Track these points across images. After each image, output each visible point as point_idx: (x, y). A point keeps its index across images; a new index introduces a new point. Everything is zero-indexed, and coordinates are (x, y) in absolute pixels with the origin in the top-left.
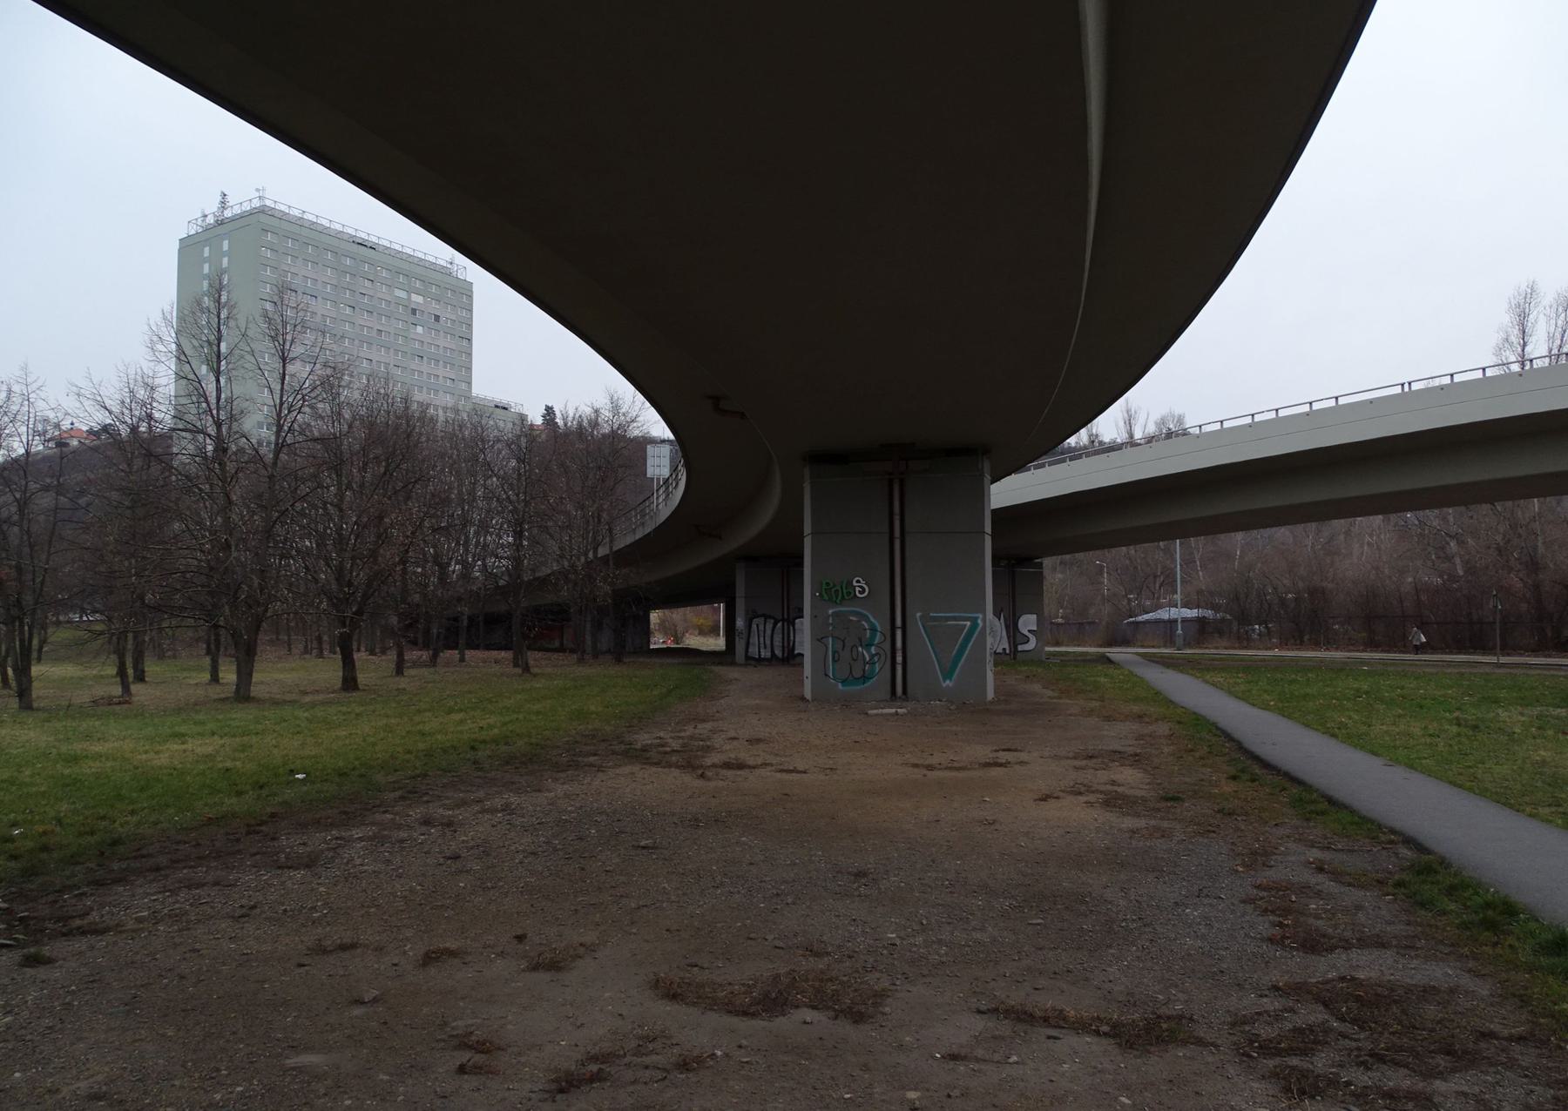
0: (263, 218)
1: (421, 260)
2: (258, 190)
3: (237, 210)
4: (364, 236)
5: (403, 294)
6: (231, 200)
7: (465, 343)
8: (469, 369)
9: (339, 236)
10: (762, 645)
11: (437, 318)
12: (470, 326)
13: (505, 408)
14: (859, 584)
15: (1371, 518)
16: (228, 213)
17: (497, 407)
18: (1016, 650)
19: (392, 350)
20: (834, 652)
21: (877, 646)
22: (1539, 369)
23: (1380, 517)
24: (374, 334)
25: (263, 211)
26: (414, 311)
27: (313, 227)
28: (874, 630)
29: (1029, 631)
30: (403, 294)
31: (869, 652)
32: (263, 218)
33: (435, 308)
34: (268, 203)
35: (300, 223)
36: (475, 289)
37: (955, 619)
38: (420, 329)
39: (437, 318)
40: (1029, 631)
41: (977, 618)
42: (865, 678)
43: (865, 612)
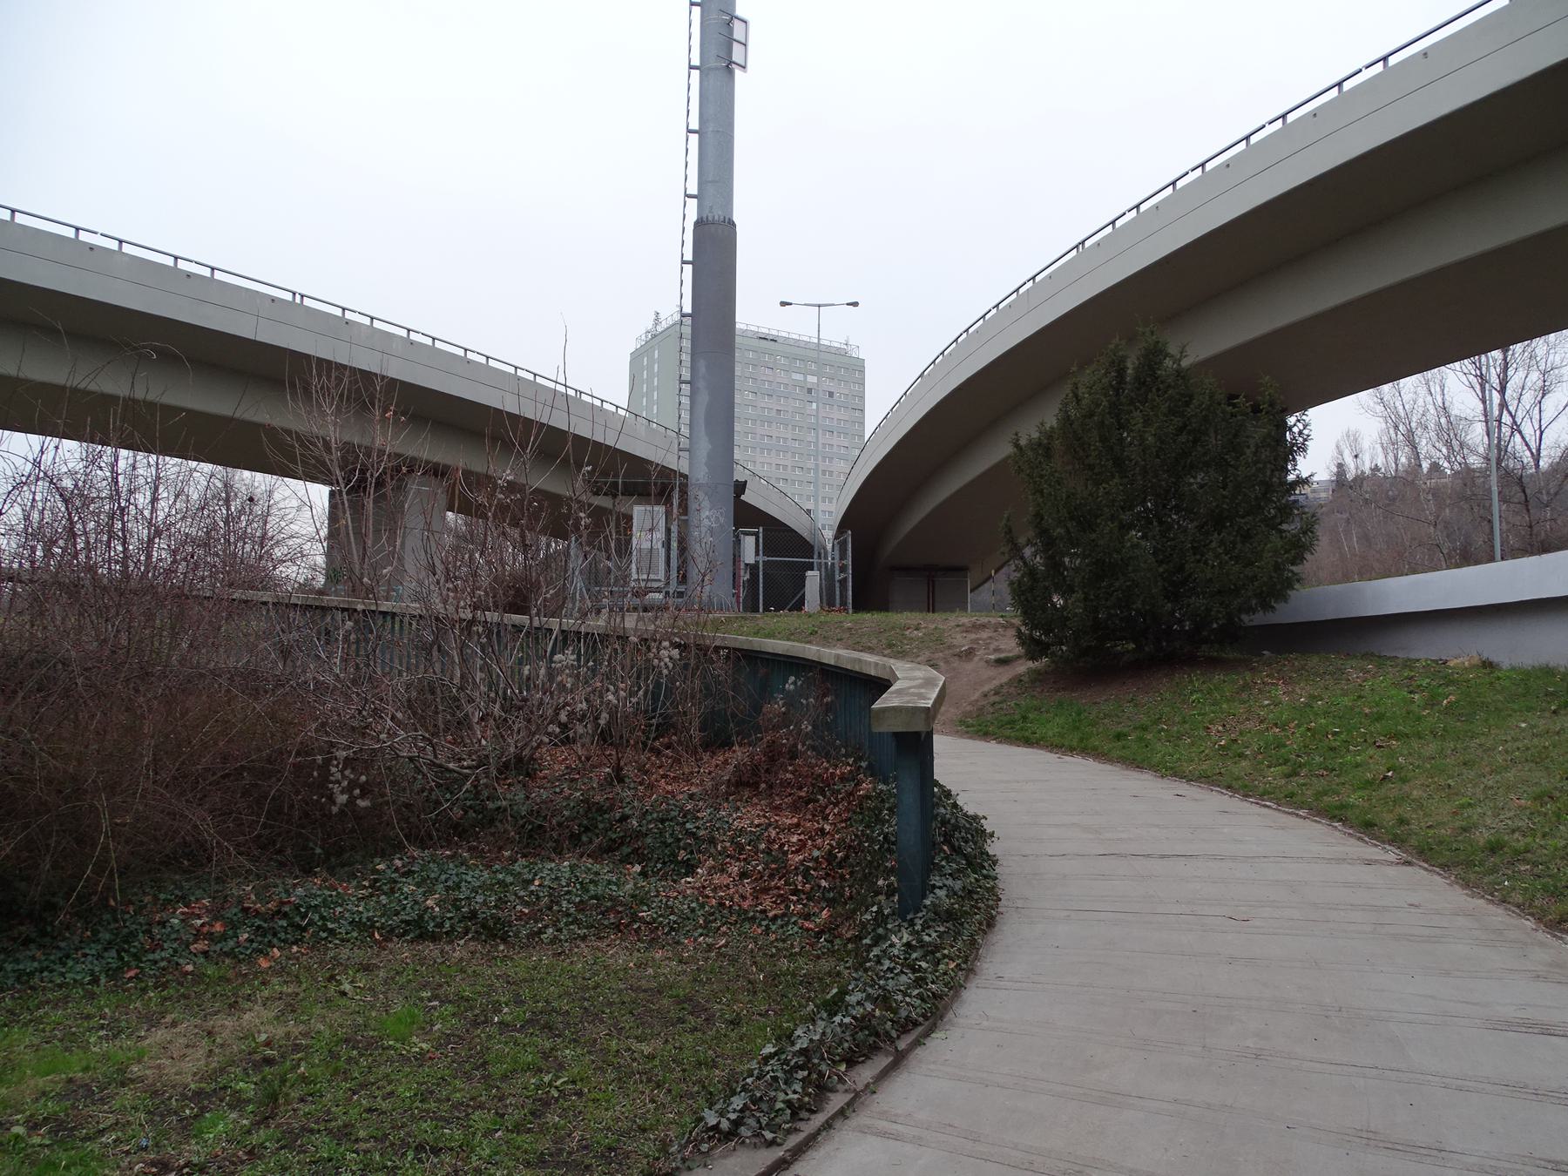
3: (664, 325)
5: (799, 377)
6: (662, 317)
11: (831, 394)
12: (862, 398)
16: (660, 329)
24: (774, 413)
26: (810, 391)
30: (799, 377)
33: (829, 385)
39: (831, 394)
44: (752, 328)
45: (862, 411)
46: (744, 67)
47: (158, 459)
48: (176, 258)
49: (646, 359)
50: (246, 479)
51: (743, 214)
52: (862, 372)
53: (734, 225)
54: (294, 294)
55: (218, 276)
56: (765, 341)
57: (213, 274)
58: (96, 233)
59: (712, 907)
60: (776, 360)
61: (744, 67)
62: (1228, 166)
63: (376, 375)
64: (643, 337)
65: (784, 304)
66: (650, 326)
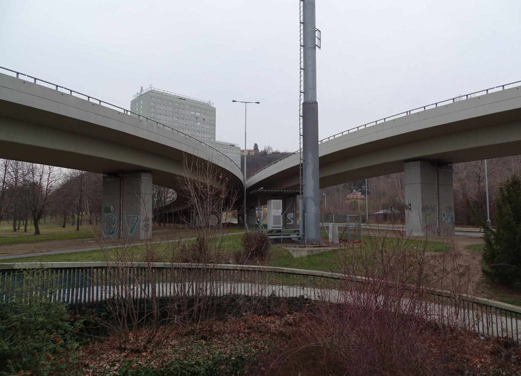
0: (151, 94)
1: (199, 102)
2: (150, 85)
3: (145, 92)
4: (181, 96)
5: (193, 113)
6: (144, 89)
7: (213, 127)
8: (215, 135)
9: (174, 97)
10: (200, 223)
11: (204, 119)
12: (215, 121)
13: (233, 146)
14: (112, 208)
15: (372, 178)
16: (143, 93)
17: (230, 145)
18: (286, 225)
19: (190, 130)
20: (106, 226)
21: (116, 224)
22: (345, 135)
23: (383, 176)
24: (184, 125)
25: (152, 91)
26: (197, 118)
27: (167, 95)
28: (115, 220)
29: (291, 218)
30: (193, 113)
31: (114, 226)
32: (151, 94)
33: (204, 116)
34: (153, 89)
35: (162, 94)
36: (216, 110)
37: (133, 217)
38: (199, 123)
39: (204, 119)
40: (291, 218)
41: (138, 217)
42: (113, 233)
43: (112, 215)
44: (177, 95)
45: (215, 126)
46: (320, 48)
47: (6, 161)
48: (35, 79)
49: (137, 103)
50: (34, 165)
51: (320, 99)
52: (215, 112)
53: (317, 103)
54: (125, 110)
55: (102, 104)
56: (181, 100)
57: (71, 93)
58: (25, 75)
59: (237, 368)
60: (185, 106)
61: (320, 48)
62: (479, 98)
63: (207, 161)
64: (136, 95)
65: (234, 101)
66: (139, 92)
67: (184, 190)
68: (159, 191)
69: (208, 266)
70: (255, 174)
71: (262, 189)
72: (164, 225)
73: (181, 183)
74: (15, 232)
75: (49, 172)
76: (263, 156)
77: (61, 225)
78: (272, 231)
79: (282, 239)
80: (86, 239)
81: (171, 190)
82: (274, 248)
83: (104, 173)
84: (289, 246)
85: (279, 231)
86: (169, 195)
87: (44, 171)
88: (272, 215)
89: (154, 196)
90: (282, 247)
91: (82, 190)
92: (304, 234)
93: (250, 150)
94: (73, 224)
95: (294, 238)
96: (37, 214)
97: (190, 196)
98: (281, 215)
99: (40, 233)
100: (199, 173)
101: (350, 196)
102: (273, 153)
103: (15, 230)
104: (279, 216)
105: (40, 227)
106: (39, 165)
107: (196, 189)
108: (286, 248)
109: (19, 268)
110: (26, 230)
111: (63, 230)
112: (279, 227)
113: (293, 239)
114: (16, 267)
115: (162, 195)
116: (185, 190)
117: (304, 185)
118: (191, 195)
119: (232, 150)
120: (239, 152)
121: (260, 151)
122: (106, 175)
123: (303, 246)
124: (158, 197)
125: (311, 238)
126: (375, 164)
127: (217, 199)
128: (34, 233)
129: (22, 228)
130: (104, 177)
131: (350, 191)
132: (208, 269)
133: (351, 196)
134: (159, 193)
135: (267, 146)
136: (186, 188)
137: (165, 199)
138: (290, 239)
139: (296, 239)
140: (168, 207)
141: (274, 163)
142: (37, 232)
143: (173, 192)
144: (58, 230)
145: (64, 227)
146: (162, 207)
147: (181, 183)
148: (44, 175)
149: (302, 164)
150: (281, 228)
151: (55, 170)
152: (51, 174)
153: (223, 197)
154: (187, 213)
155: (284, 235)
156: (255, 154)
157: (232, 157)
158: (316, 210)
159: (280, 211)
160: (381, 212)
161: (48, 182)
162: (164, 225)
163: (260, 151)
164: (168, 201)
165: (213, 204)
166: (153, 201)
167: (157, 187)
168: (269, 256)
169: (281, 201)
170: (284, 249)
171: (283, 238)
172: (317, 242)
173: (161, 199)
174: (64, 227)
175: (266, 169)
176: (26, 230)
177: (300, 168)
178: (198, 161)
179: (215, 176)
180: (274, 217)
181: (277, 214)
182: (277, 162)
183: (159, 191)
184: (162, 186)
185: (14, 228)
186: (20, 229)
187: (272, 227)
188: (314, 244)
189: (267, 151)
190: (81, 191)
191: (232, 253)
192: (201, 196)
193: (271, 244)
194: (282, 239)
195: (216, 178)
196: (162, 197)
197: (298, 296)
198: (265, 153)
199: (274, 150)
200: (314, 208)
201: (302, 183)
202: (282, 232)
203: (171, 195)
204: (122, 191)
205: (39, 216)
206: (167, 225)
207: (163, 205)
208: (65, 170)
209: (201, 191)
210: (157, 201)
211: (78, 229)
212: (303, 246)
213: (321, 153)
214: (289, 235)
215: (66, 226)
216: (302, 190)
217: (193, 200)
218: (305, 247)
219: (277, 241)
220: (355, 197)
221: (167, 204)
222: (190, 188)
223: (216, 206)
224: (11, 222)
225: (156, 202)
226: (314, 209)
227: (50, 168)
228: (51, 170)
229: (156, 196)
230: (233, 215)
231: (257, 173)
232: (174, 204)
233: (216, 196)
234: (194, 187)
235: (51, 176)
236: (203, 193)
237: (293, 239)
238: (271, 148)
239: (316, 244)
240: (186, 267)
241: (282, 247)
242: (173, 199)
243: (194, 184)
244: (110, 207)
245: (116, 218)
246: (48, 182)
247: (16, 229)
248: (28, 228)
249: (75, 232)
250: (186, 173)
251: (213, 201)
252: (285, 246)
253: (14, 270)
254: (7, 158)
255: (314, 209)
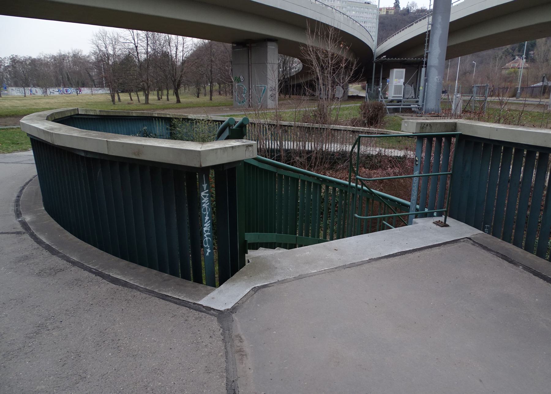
13: (368, 3)
14: (241, 77)
17: (365, 3)
50: (170, 35)
67: (307, 59)
68: (285, 60)
69: (325, 126)
70: (387, 40)
71: (384, 58)
72: (290, 97)
73: (304, 52)
74: (159, 101)
75: (183, 43)
76: (404, 15)
77: (195, 95)
78: (392, 101)
79: (400, 108)
80: (221, 107)
81: (296, 59)
82: (389, 117)
83: (233, 43)
84: (406, 115)
85: (399, 101)
86: (294, 65)
87: (179, 42)
88: (394, 85)
89: (279, 67)
90: (399, 116)
91: (212, 60)
92: (423, 104)
93: (389, 8)
94: (205, 95)
95: (415, 108)
96: (176, 84)
97: (312, 65)
98: (403, 84)
99: (181, 102)
100: (321, 42)
101: (511, 65)
102: (418, 11)
103: (159, 99)
104: (401, 86)
105: (180, 97)
106: (173, 36)
107: (318, 58)
108: (403, 117)
109: (191, 118)
110: (168, 100)
111: (198, 100)
112: (400, 97)
113: (413, 109)
114: (189, 117)
115: (287, 65)
116: (308, 60)
117: (429, 52)
118: (313, 64)
119: (366, 10)
120: (375, 11)
121: (401, 9)
122: (235, 45)
123: (420, 115)
124: (283, 67)
125: (430, 108)
126: (527, 25)
127: (337, 68)
128: (176, 102)
129: (164, 97)
130: (233, 47)
131: (512, 58)
132: (323, 129)
133: (512, 64)
134: (284, 63)
135: (410, 2)
136: (308, 58)
137: (290, 69)
138: (410, 109)
139: (416, 109)
140: (292, 78)
141: (409, 27)
142: (178, 101)
143: (299, 62)
144: (194, 100)
145: (198, 97)
146: (288, 78)
147: (304, 52)
148: (179, 46)
149: (429, 31)
150: (402, 98)
151: (188, 40)
152: (185, 44)
153: (344, 65)
154: (312, 85)
155: (403, 105)
156: (395, 13)
157: (367, 18)
158: (438, 80)
159: (403, 80)
160: (540, 84)
161: (183, 53)
162: (290, 97)
163: (401, 9)
164: (294, 72)
165: (334, 73)
166: (279, 71)
167: (282, 57)
168: (385, 124)
169: (404, 70)
170: (400, 117)
171: (402, 108)
172: (436, 112)
173: (286, 68)
174: (198, 97)
175: (400, 33)
176: (168, 100)
177: (427, 34)
178: (321, 30)
179: (336, 44)
180: (396, 86)
181: (399, 84)
182: (413, 24)
183: (285, 60)
184: (287, 55)
185: (158, 97)
186: (162, 98)
187: (393, 97)
188: (432, 114)
189: (411, 8)
190: (212, 61)
191: (349, 120)
192: (322, 65)
193: (388, 113)
194: (400, 108)
195: (337, 48)
196: (287, 67)
197: (402, 156)
198: (407, 11)
199: (419, 7)
200: (437, 77)
201: (428, 50)
202: (402, 102)
203: (296, 65)
204: (250, 61)
205: (179, 86)
206: (292, 96)
207: (289, 76)
208: (196, 40)
209: (323, 60)
210: (283, 71)
211: (211, 99)
212: (420, 115)
213: (454, 17)
214: (410, 105)
215: (199, 97)
216: (427, 57)
217: (315, 69)
218: (422, 116)
219: (396, 110)
220: (517, 66)
221: (292, 75)
222: (313, 58)
223: (336, 75)
224: (156, 92)
225: (281, 73)
226: (437, 79)
227: (183, 38)
228: (184, 40)
229: (281, 66)
230: (364, 88)
231: (389, 39)
232: (299, 74)
233: (337, 65)
234: (316, 56)
235: (185, 46)
236: (324, 62)
237: (413, 109)
238: (416, 5)
239: (434, 114)
240: (306, 126)
241: (399, 116)
242: (298, 69)
243: (316, 53)
244: (240, 78)
245: (245, 87)
246: (183, 53)
247: (159, 98)
248: (169, 97)
249: (209, 102)
250: (309, 41)
251: (334, 69)
252: (401, 115)
253: (189, 119)
254: (147, 31)
255: (437, 79)
